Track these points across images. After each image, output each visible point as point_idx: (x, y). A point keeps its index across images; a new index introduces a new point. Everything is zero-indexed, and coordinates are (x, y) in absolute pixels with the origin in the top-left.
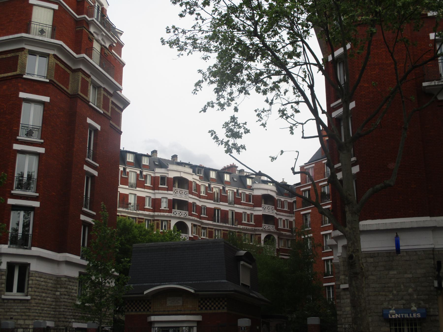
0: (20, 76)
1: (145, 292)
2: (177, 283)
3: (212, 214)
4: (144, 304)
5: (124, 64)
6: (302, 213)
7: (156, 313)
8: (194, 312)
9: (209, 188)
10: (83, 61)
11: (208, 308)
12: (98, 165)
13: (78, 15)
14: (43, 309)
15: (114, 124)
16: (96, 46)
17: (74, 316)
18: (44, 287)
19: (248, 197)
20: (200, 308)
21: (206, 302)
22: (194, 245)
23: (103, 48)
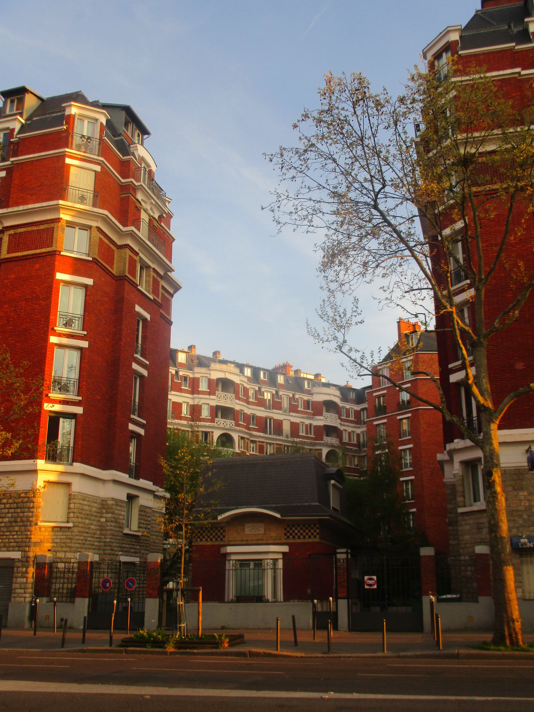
0: (54, 254)
1: (220, 518)
3: (262, 424)
4: (217, 531)
5: (174, 240)
6: (375, 423)
8: (279, 541)
9: (259, 392)
10: (132, 235)
12: (148, 363)
13: (123, 178)
16: (144, 216)
17: (122, 547)
18: (88, 512)
19: (307, 404)
20: (286, 537)
21: (294, 529)
22: (243, 464)
23: (151, 219)
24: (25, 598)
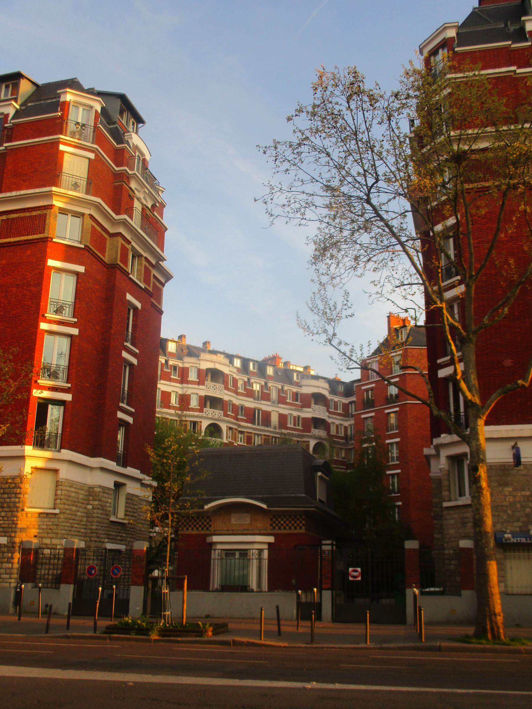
0: (46, 240)
1: (206, 507)
2: (251, 496)
3: (251, 415)
4: (203, 520)
5: (167, 229)
7: (217, 532)
8: (265, 532)
10: (125, 224)
11: (282, 527)
13: (117, 166)
14: (72, 525)
15: (154, 302)
16: (137, 205)
17: (108, 535)
19: (296, 396)
20: (272, 527)
21: (280, 519)
23: (144, 208)
24: (10, 583)
